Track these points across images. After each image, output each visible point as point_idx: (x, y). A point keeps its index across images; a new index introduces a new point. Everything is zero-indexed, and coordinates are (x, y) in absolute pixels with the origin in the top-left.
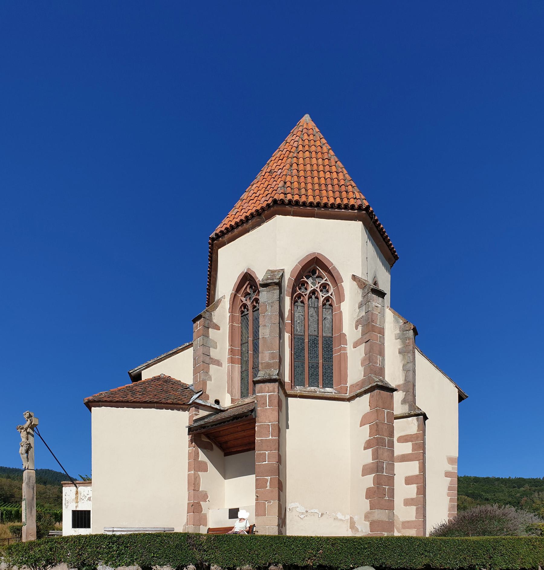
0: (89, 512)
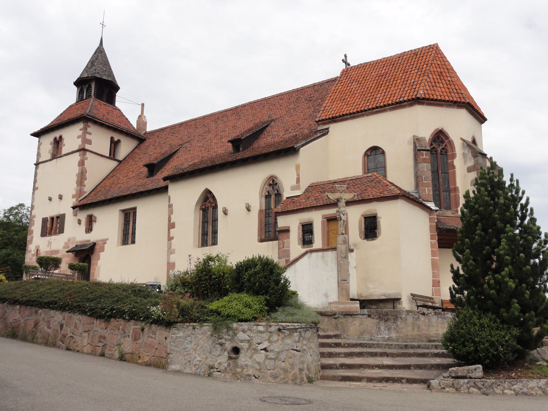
0: (43, 218)
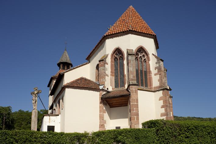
0: (54, 126)
